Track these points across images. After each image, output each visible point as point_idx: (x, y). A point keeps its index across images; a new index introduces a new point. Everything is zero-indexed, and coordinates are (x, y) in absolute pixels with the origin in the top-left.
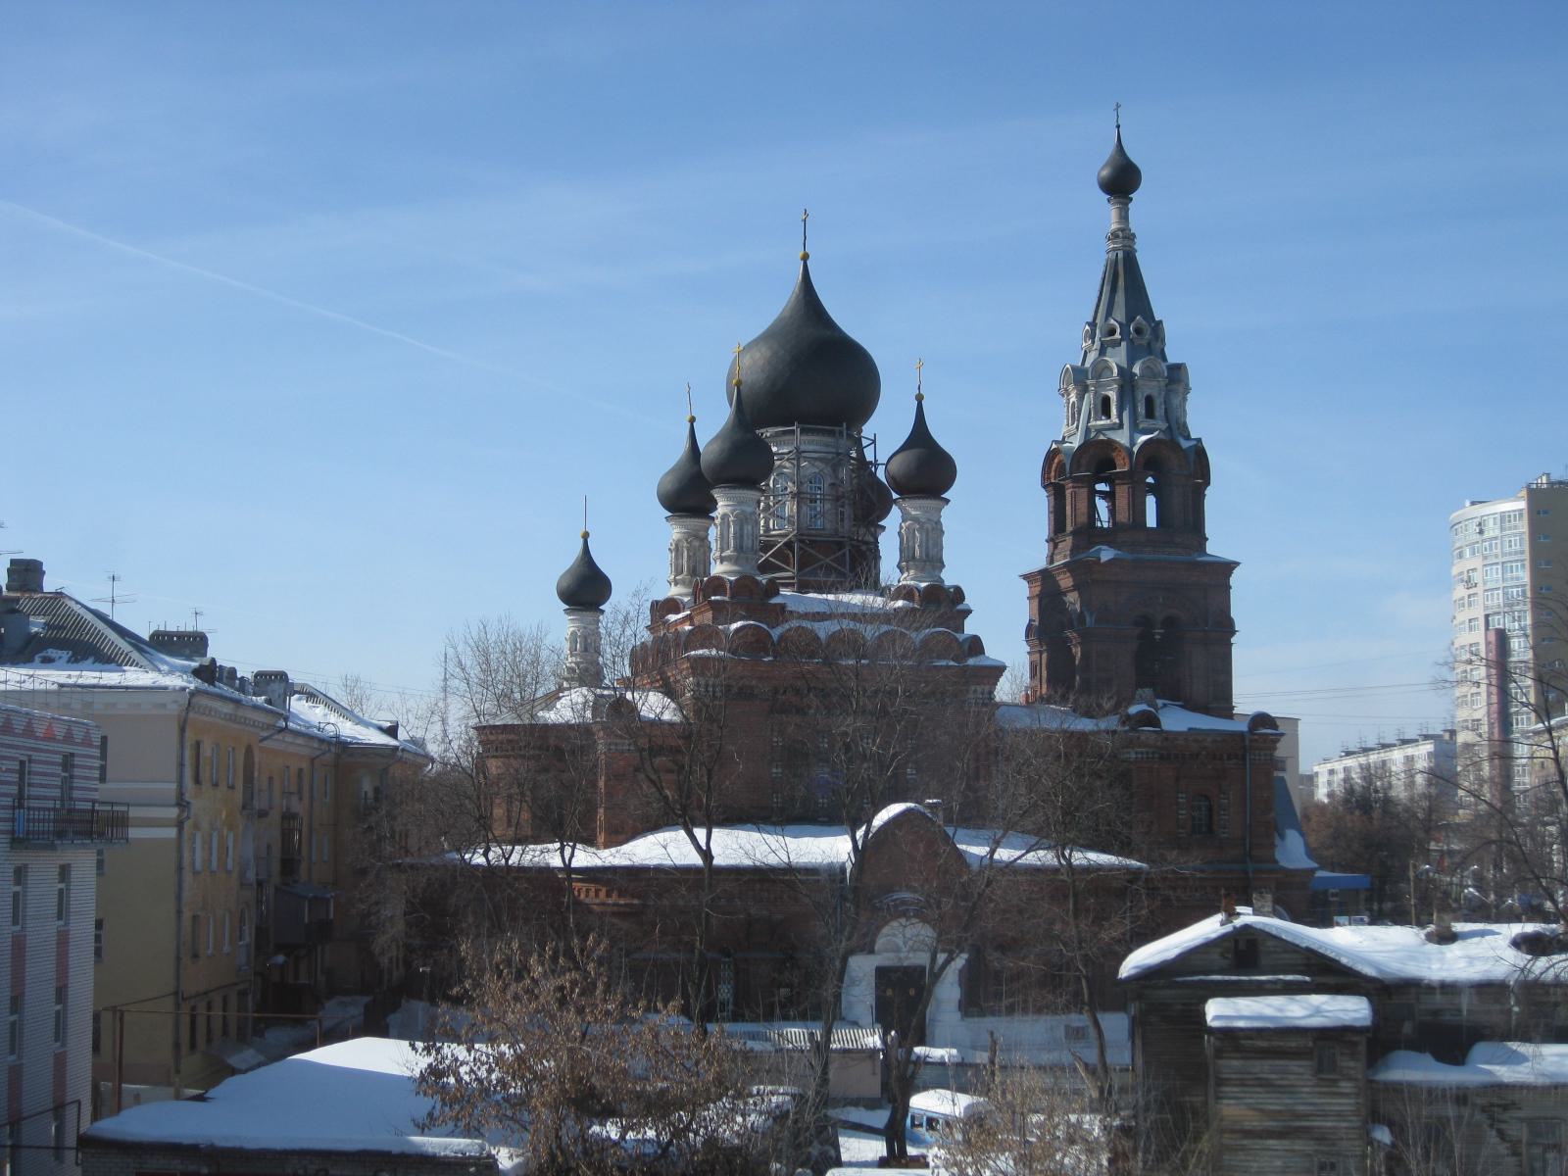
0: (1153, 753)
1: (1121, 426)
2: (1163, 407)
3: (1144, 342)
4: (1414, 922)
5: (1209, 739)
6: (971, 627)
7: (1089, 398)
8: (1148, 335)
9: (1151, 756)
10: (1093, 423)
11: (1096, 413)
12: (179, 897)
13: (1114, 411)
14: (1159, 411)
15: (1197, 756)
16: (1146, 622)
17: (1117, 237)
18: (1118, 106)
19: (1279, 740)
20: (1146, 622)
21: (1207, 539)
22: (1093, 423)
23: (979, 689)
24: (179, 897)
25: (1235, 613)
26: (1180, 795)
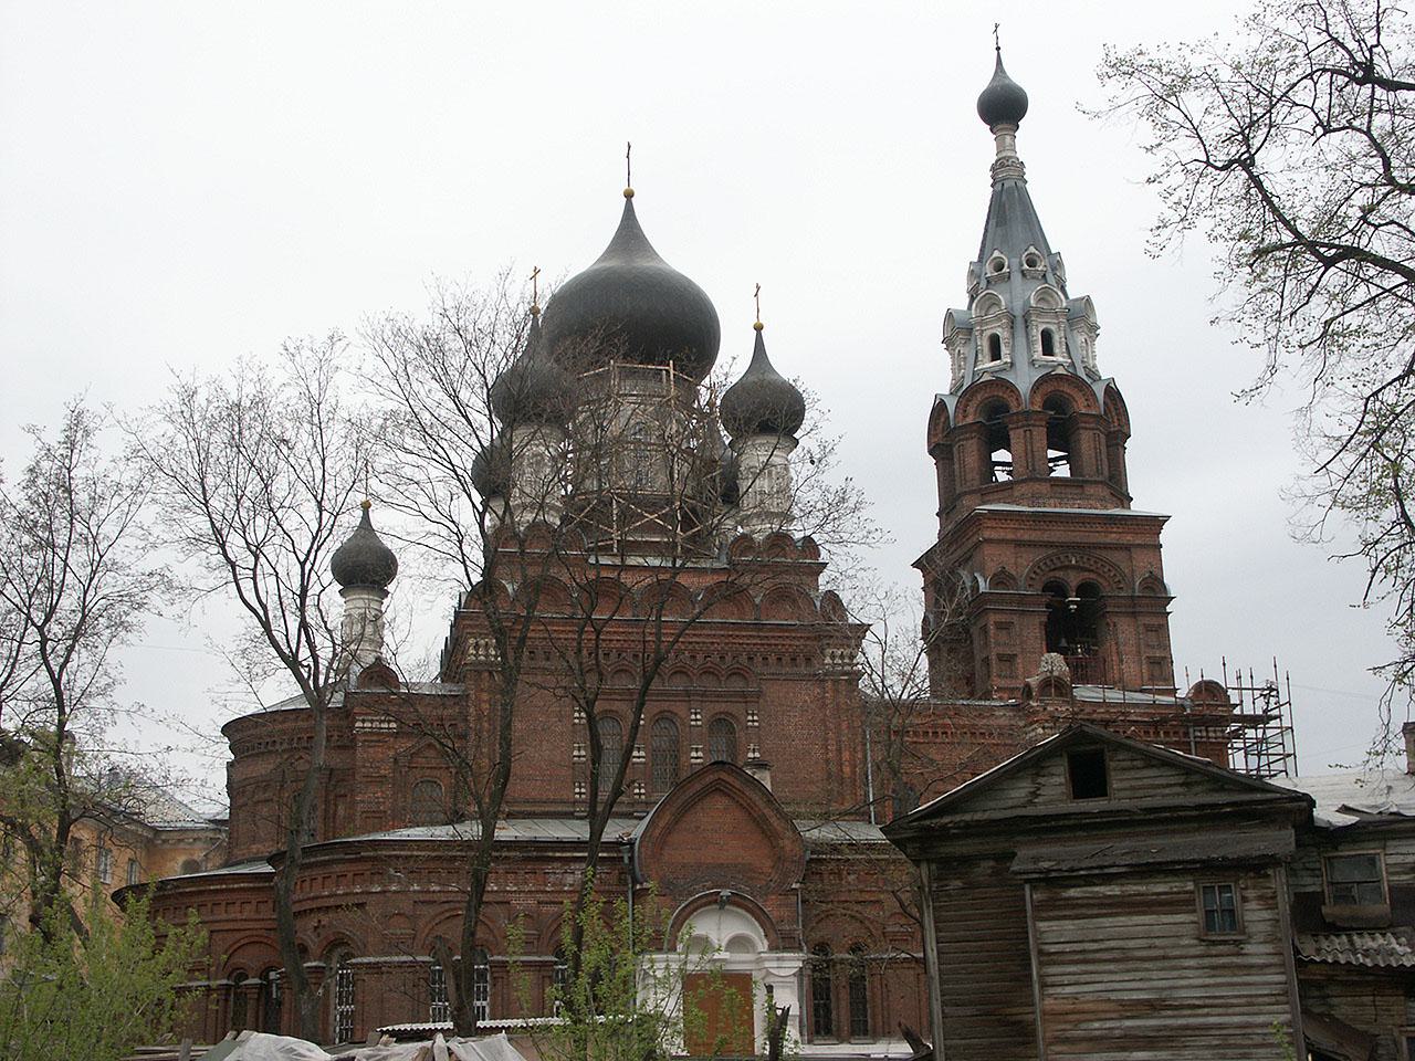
13: (1004, 350)
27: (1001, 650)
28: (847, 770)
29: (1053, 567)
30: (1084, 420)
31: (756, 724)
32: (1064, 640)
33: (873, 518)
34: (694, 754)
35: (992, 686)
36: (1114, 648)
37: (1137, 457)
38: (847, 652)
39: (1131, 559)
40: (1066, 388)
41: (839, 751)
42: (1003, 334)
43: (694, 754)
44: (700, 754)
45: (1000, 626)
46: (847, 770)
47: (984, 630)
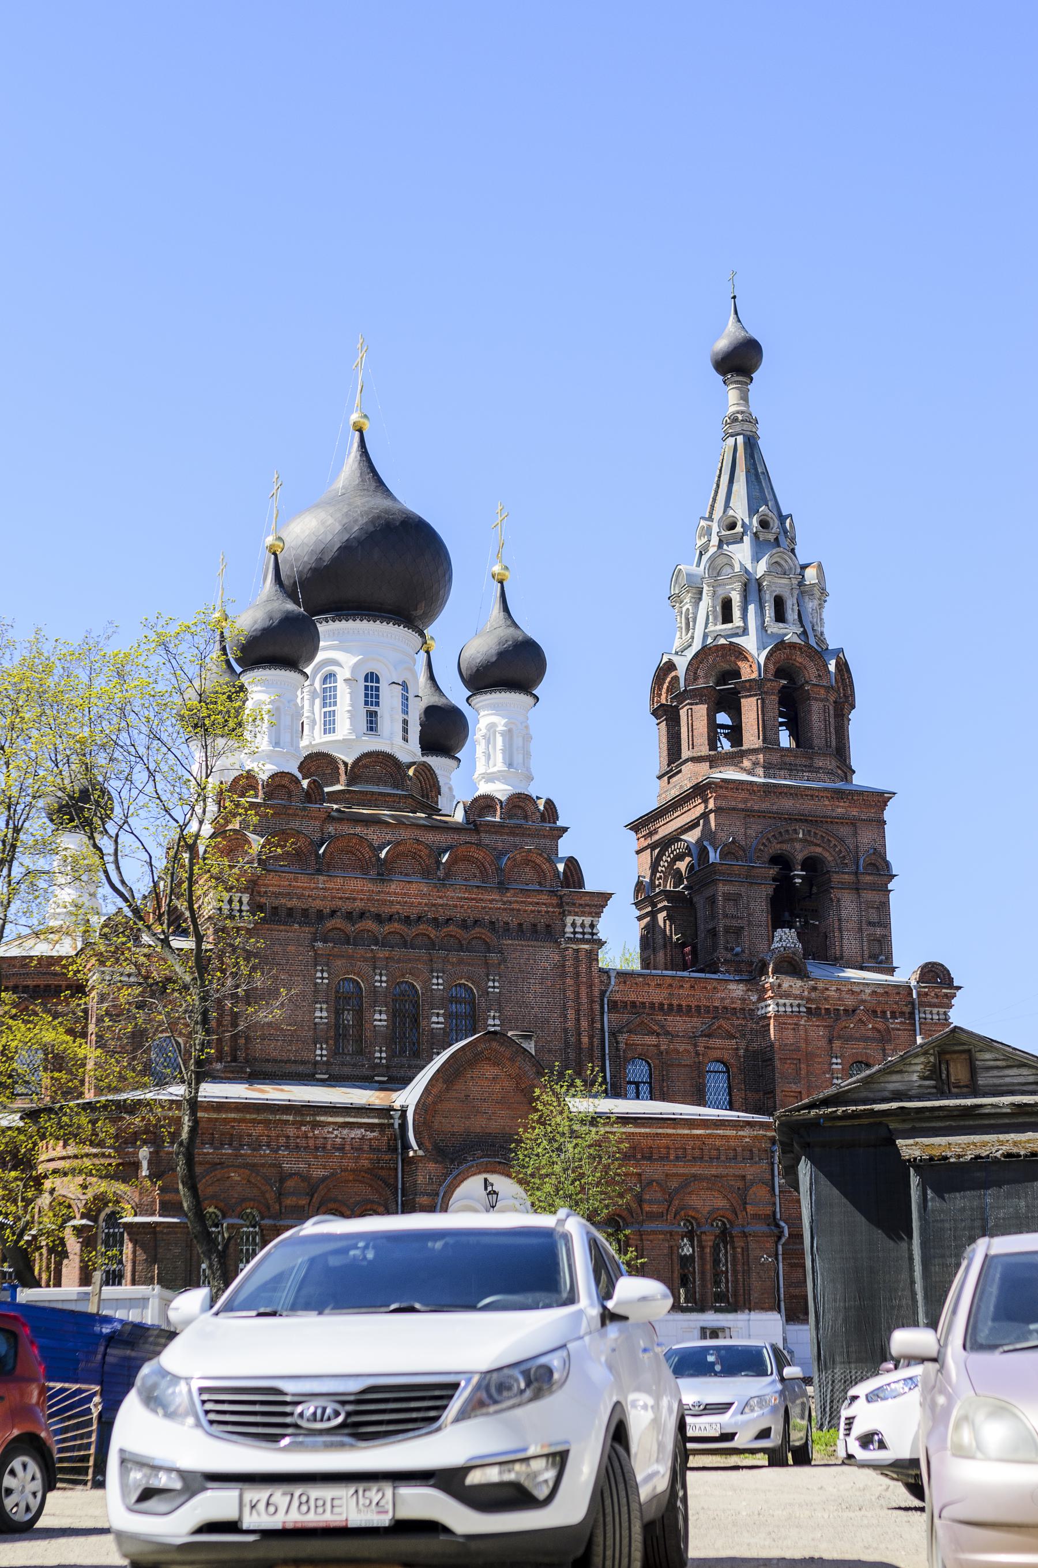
0: (799, 1006)
1: (745, 631)
2: (796, 608)
3: (771, 537)
4: (922, 1318)
5: (868, 991)
6: (566, 847)
7: (706, 602)
8: (775, 524)
9: (796, 1009)
10: (711, 628)
11: (715, 618)
12: (907, 1509)
13: (736, 613)
14: (791, 615)
15: (854, 1011)
16: (781, 861)
17: (736, 420)
18: (734, 273)
19: (954, 996)
20: (781, 861)
21: (854, 772)
22: (711, 628)
23: (579, 920)
24: (907, 1509)
25: (893, 855)
26: (834, 1060)
27: (728, 922)
28: (585, 1040)
29: (780, 839)
30: (808, 694)
31: (497, 990)
32: (787, 914)
33: (597, 777)
34: (434, 1019)
35: (718, 959)
36: (836, 924)
37: (859, 726)
38: (588, 920)
39: (855, 834)
40: (800, 659)
41: (578, 1020)
42: (736, 598)
43: (434, 1019)
44: (441, 1019)
45: (728, 898)
46: (585, 1040)
47: (712, 901)
